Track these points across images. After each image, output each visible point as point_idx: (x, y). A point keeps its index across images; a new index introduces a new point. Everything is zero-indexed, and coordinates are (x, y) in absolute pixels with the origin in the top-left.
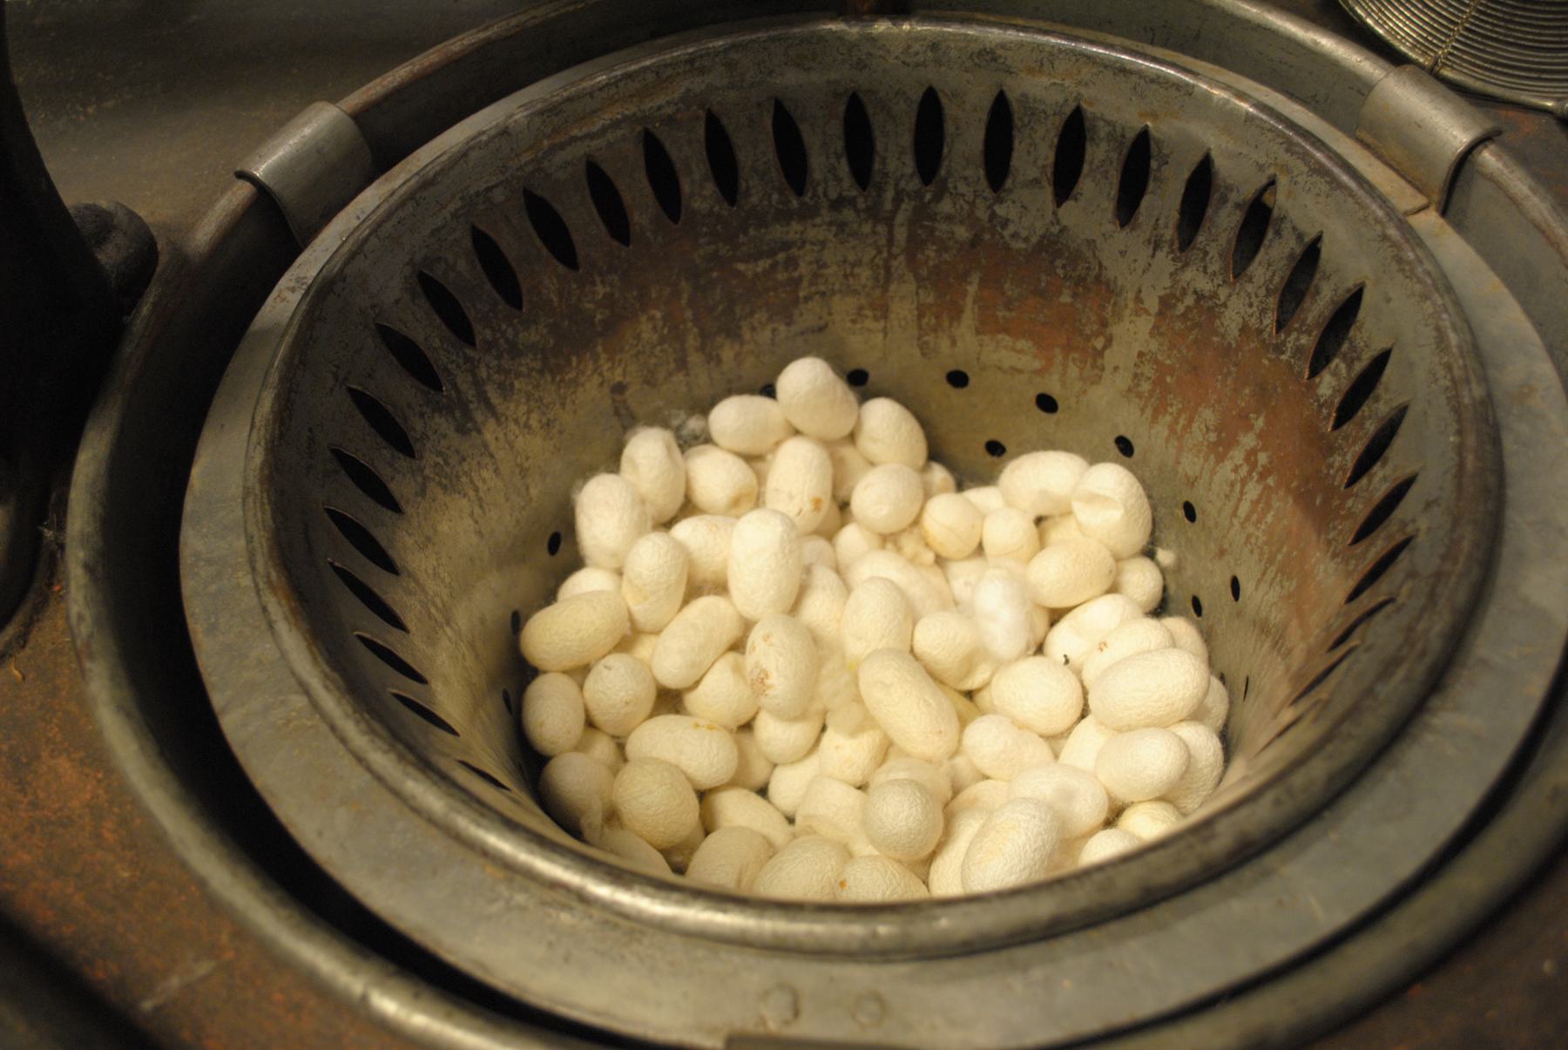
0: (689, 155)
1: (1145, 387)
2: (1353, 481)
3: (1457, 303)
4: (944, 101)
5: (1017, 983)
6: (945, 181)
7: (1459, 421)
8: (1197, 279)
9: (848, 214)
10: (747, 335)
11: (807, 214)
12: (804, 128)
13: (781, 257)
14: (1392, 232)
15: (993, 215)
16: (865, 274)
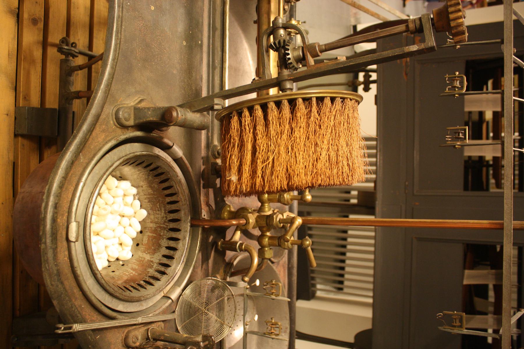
0: (173, 198)
1: (140, 259)
2: (130, 285)
3: (153, 297)
4: (179, 232)
5: (81, 251)
6: (169, 232)
7: (139, 297)
8: (155, 265)
9: (165, 219)
10: (149, 203)
11: (165, 213)
12: (177, 213)
13: (159, 209)
14: (161, 289)
15: (164, 238)
16: (156, 220)
